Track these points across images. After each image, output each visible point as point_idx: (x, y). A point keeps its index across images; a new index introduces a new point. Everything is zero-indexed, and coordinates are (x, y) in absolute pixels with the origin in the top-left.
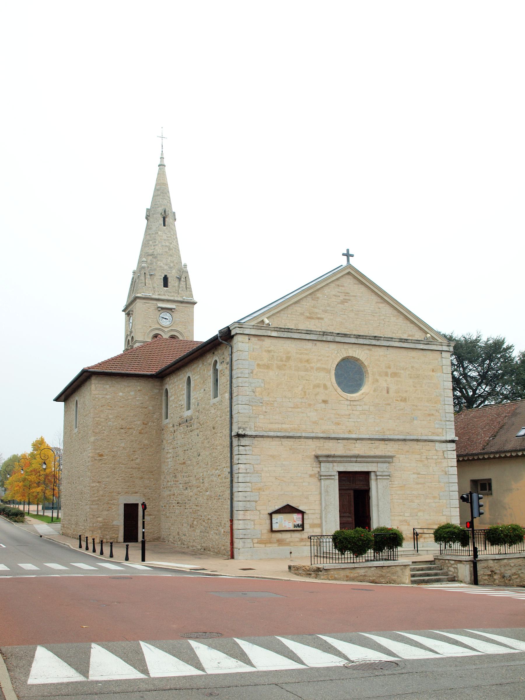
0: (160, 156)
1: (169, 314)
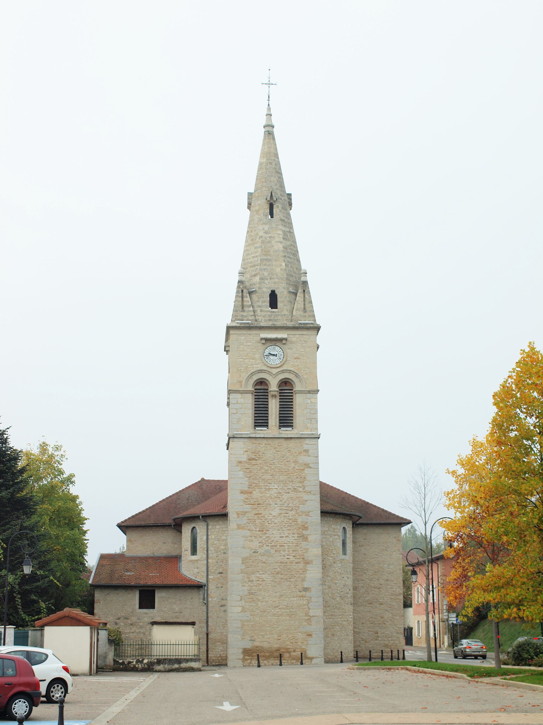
0: (266, 112)
1: (279, 348)
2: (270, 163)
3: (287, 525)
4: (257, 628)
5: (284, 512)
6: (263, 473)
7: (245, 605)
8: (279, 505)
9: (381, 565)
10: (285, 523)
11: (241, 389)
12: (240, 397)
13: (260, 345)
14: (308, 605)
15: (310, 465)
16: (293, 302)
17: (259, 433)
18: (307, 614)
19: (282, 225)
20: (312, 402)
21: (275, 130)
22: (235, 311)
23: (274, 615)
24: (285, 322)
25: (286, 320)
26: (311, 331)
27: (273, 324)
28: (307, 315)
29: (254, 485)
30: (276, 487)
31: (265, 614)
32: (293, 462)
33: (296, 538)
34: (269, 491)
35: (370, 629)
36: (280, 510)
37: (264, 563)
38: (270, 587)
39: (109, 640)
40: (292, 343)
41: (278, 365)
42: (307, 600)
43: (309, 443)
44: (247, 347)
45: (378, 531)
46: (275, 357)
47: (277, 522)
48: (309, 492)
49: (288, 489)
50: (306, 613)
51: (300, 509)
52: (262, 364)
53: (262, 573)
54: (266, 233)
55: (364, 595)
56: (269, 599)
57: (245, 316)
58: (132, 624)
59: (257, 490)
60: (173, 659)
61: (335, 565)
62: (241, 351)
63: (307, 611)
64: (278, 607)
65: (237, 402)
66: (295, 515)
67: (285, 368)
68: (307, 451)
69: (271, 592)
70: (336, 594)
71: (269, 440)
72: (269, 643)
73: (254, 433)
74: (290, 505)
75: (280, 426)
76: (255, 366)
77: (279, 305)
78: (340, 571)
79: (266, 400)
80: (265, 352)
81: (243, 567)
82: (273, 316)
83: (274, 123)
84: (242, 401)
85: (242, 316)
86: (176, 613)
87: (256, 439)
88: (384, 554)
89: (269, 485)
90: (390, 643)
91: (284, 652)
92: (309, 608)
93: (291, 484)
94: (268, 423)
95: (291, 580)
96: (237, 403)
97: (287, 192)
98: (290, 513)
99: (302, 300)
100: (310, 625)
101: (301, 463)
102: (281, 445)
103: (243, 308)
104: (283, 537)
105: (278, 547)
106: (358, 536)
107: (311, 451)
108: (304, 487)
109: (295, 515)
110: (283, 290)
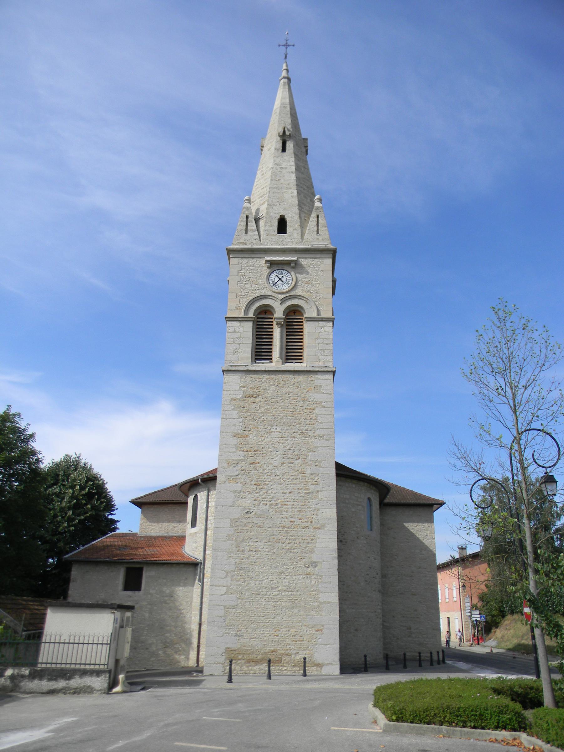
5: (287, 461)
16: (303, 226)
20: (325, 332)
28: (320, 238)
33: (302, 495)
41: (286, 290)
67: (293, 293)
75: (287, 359)
76: (257, 291)
77: (289, 229)
84: (241, 330)
96: (235, 332)
97: (303, 136)
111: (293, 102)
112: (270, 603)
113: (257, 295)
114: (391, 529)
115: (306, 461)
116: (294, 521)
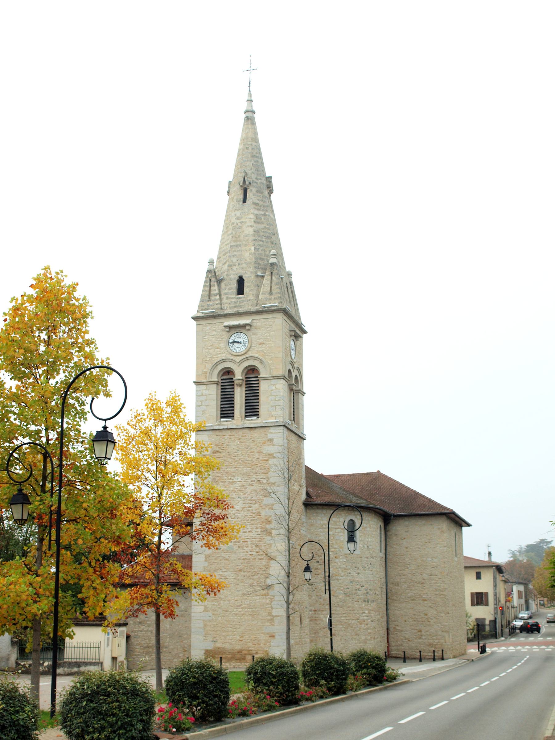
0: (247, 98)
1: (244, 335)
2: (246, 148)
3: (250, 519)
4: (219, 628)
5: (247, 505)
6: (226, 466)
7: (208, 604)
8: (243, 499)
9: (425, 559)
10: (249, 518)
11: (205, 381)
12: (205, 388)
13: (225, 333)
14: (271, 604)
15: (274, 455)
17: (223, 425)
18: (270, 614)
19: (255, 208)
20: (276, 389)
21: (255, 115)
22: (202, 301)
23: (236, 615)
24: (250, 307)
25: (252, 305)
26: (277, 314)
27: (238, 311)
29: (218, 478)
30: (240, 480)
31: (227, 613)
32: (257, 452)
33: (259, 533)
34: (232, 484)
35: (413, 627)
36: (244, 503)
37: (227, 559)
38: (232, 585)
39: (12, 641)
40: (257, 328)
41: (243, 353)
42: (270, 598)
43: (273, 431)
44: (213, 337)
45: (420, 522)
46: (239, 344)
47: (240, 517)
48: (273, 484)
49: (252, 481)
50: (268, 613)
51: (264, 502)
52: (227, 352)
53: (225, 570)
54: (237, 219)
55: (407, 591)
56: (231, 598)
57: (212, 305)
58: (140, 623)
59: (221, 484)
60: (72, 663)
61: (337, 560)
62: (207, 341)
63: (270, 610)
64: (240, 606)
65: (202, 394)
66: (258, 509)
67: (249, 354)
68: (271, 440)
69: (233, 591)
70: (338, 591)
71: (233, 431)
72: (231, 644)
73: (219, 425)
74: (254, 498)
77: (246, 290)
78: (344, 566)
79: (232, 390)
80: (230, 340)
81: (206, 564)
82: (238, 303)
83: (255, 109)
84: (207, 392)
85: (208, 305)
86: (182, 611)
87: (220, 431)
88: (427, 547)
89: (233, 478)
90: (434, 642)
91: (246, 654)
92: (272, 608)
93: (254, 476)
94: (233, 413)
95: (254, 577)
96: (202, 395)
97: (268, 175)
98: (254, 506)
99: (269, 282)
100: (273, 625)
101: (265, 453)
102: (246, 436)
103: (209, 298)
104: (246, 532)
105: (241, 542)
106: (400, 529)
107: (275, 440)
108: (268, 478)
109: (258, 509)
110: (251, 275)
111: (255, 140)
112: (236, 617)
113: (219, 359)
114: (404, 539)
115: (262, 505)
116: (252, 554)
